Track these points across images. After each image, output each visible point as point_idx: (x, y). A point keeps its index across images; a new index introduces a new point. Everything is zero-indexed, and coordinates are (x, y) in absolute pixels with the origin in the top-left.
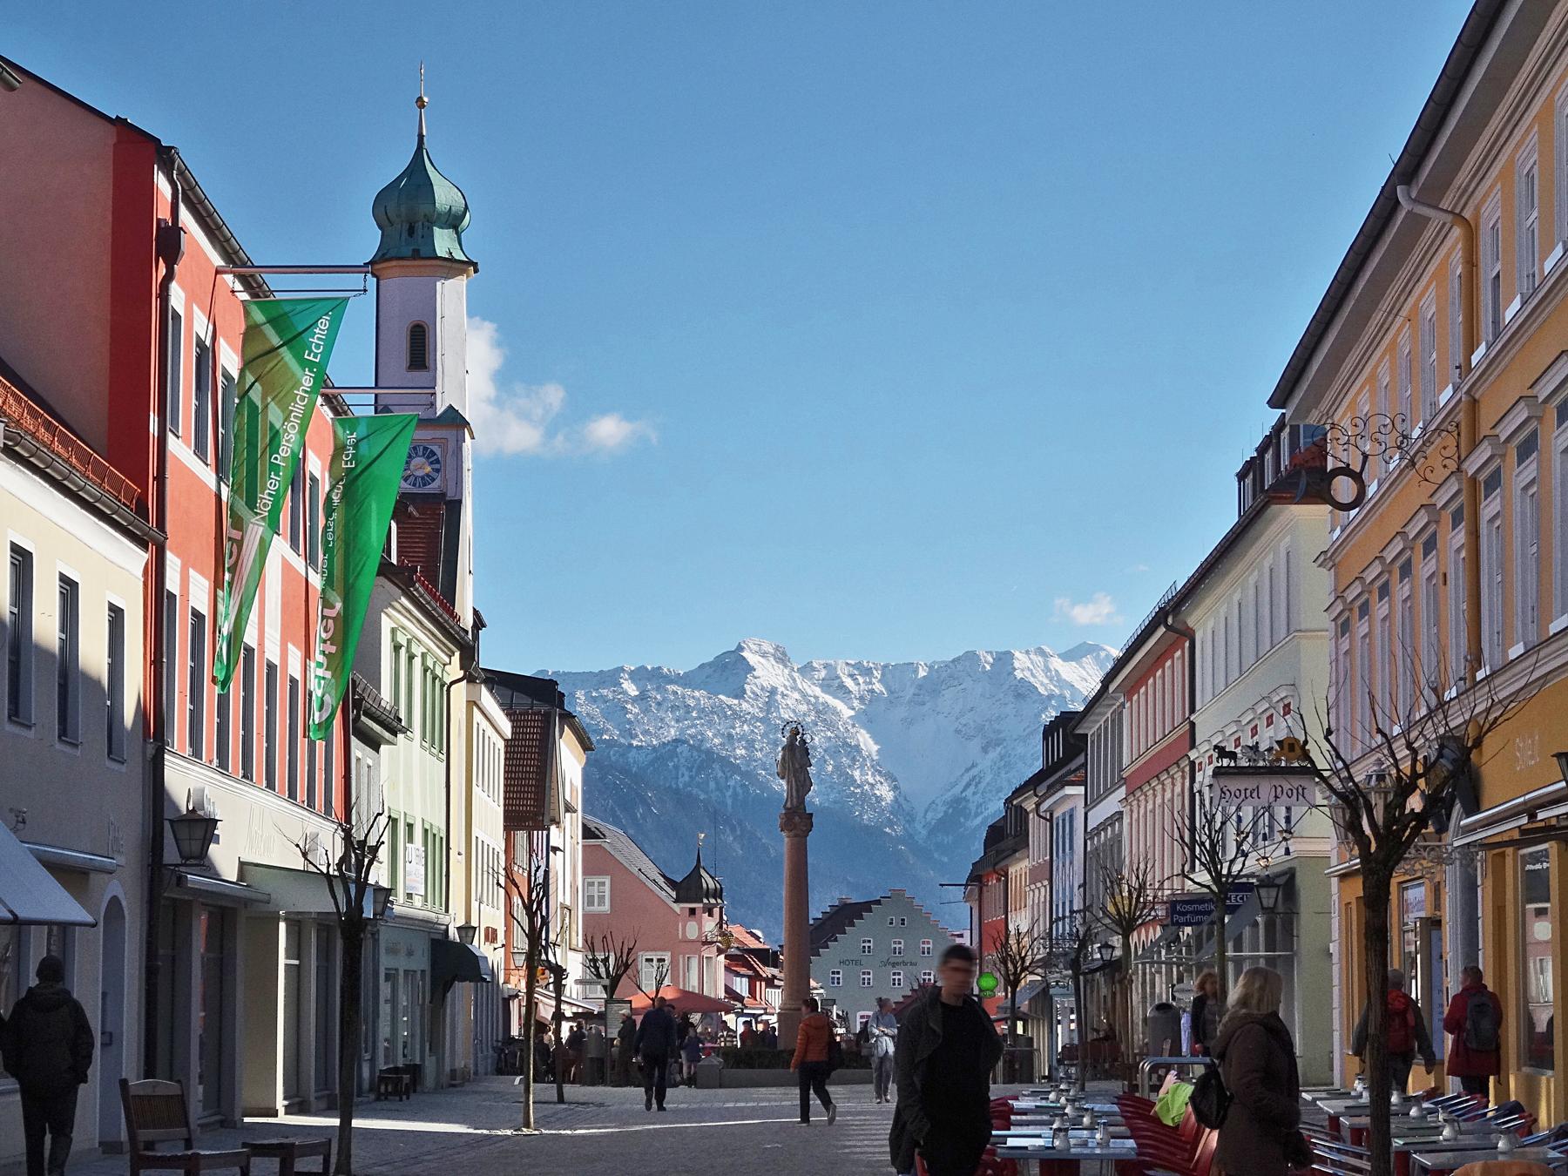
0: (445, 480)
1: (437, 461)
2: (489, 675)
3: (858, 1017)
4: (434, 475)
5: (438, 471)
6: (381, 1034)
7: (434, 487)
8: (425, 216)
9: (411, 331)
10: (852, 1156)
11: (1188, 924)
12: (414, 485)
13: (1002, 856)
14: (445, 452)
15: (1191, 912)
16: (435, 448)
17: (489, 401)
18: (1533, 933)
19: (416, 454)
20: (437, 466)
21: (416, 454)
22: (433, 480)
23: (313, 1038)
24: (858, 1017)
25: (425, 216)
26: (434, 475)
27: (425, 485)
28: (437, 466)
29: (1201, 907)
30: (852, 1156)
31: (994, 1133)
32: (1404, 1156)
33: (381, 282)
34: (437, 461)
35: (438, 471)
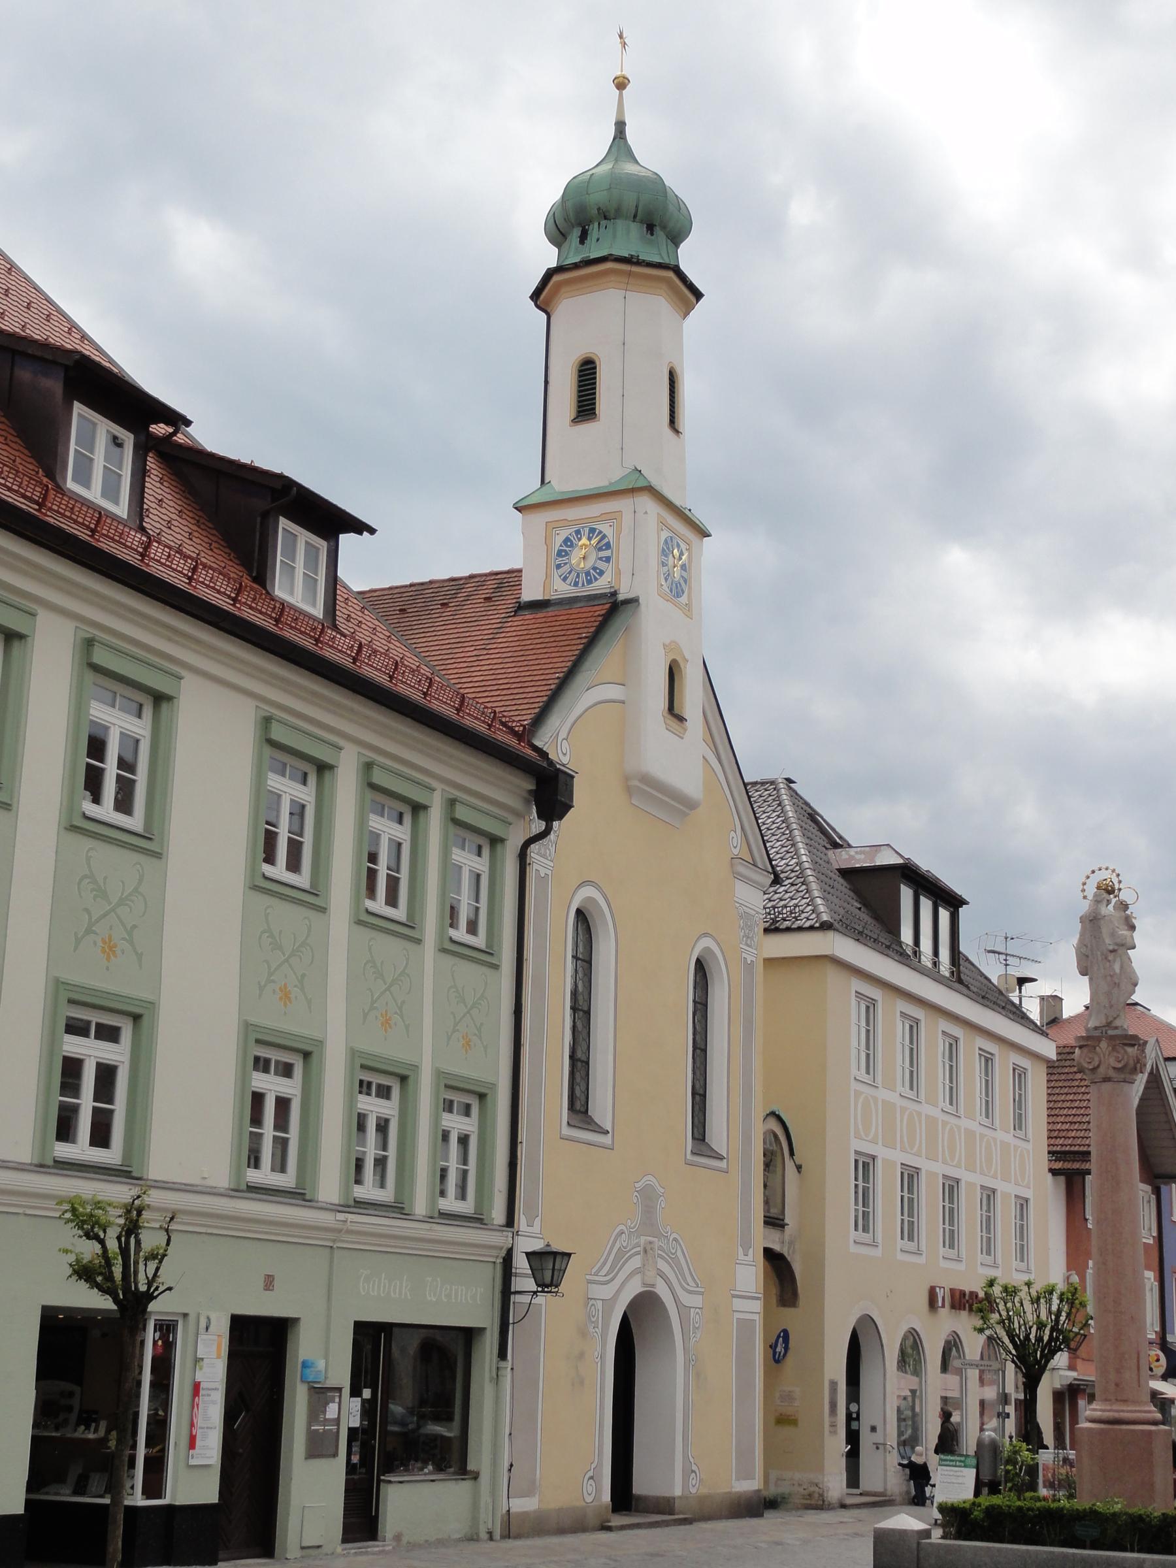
0: (618, 573)
5: (608, 559)
7: (601, 585)
19: (601, 559)
20: (607, 553)
21: (601, 559)
22: (601, 573)
26: (602, 565)
27: (590, 582)
28: (607, 553)
35: (608, 559)
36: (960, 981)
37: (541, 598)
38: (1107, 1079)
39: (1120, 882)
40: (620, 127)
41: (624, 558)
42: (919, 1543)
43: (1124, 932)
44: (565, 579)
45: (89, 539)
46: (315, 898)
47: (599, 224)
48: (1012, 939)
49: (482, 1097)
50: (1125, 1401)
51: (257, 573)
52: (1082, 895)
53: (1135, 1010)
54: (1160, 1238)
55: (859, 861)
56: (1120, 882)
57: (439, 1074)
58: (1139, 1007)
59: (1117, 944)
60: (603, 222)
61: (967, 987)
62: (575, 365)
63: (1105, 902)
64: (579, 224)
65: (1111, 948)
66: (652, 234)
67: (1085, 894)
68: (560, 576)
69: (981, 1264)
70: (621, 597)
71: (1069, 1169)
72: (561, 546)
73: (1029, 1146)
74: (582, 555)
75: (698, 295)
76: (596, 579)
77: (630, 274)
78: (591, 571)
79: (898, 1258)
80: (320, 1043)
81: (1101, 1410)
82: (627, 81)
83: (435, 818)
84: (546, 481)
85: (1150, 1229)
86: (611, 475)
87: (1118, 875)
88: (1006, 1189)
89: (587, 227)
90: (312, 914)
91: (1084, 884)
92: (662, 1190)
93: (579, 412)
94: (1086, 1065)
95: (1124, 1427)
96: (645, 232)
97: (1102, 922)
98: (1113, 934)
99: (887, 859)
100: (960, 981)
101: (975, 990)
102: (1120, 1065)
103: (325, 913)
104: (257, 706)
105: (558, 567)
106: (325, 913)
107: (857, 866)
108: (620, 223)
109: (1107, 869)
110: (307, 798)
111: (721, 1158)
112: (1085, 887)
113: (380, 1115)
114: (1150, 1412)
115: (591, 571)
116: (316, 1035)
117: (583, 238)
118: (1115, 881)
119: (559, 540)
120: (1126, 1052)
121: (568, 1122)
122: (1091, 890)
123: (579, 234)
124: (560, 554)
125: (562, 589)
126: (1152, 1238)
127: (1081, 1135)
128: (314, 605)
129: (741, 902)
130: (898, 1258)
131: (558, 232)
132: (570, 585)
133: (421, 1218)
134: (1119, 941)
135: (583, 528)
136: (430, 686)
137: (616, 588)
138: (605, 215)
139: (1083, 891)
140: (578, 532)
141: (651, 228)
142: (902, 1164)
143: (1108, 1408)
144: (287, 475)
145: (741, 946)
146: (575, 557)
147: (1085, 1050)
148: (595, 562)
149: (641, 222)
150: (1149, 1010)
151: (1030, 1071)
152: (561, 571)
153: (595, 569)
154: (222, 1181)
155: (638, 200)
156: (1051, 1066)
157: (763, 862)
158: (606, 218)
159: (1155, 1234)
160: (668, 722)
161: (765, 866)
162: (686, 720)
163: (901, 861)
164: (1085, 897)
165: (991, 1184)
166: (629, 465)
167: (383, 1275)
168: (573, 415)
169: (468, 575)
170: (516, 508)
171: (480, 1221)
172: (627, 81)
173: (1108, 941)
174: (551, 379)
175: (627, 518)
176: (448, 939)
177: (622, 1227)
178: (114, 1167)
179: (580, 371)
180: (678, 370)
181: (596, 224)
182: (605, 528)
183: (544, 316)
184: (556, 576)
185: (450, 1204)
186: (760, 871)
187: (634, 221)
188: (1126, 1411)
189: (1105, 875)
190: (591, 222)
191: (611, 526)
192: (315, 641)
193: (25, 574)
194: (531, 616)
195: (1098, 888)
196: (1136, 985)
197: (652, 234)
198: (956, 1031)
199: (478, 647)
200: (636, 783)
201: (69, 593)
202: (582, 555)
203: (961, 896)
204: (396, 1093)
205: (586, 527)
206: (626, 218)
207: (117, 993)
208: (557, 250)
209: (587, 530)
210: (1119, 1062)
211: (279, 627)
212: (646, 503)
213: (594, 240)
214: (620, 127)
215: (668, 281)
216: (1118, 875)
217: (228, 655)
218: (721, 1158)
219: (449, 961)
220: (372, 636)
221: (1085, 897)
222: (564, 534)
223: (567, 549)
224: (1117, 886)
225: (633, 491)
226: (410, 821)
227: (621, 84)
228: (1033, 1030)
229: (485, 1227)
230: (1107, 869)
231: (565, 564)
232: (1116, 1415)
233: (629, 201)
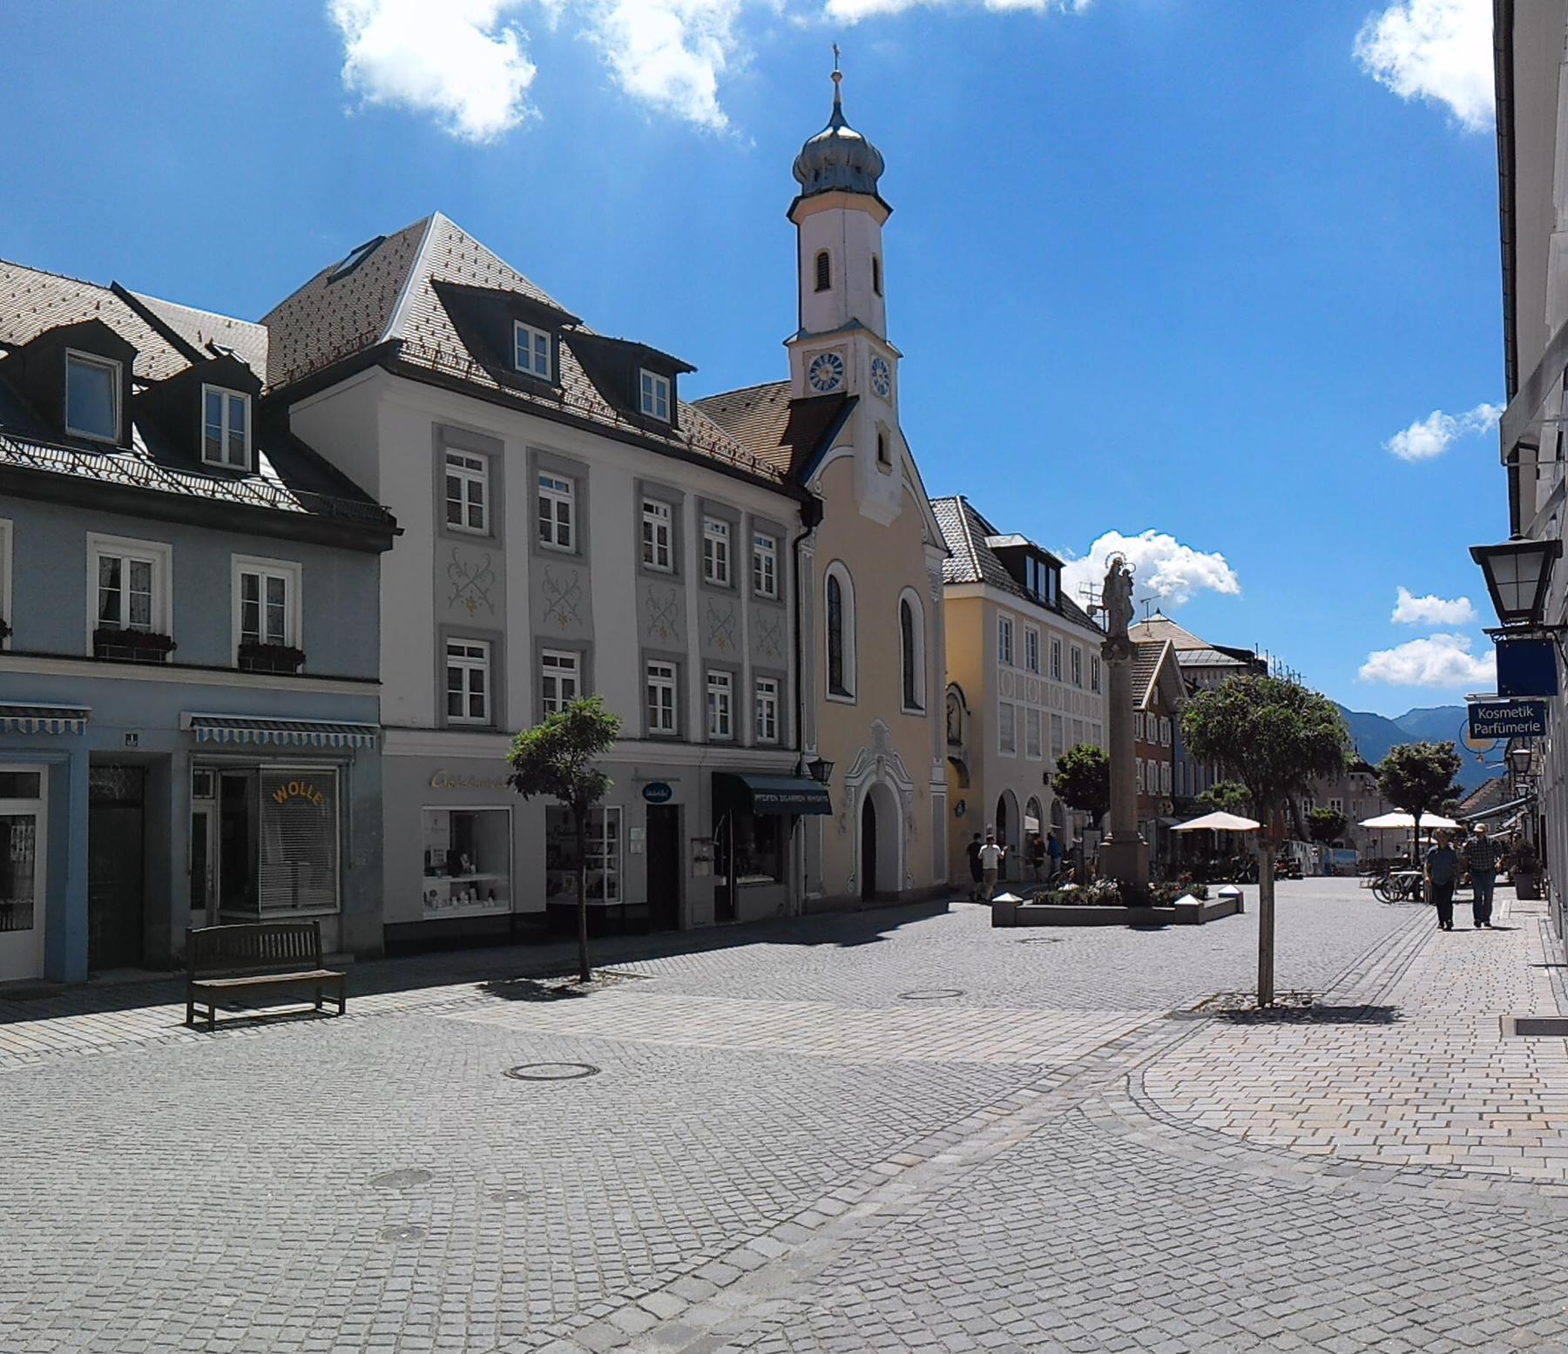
1: (840, 365)
2: (1223, 777)
4: (837, 376)
5: (840, 373)
6: (686, 834)
7: (837, 389)
8: (825, 159)
9: (819, 259)
12: (822, 389)
13: (894, 400)
15: (1499, 720)
16: (837, 354)
17: (522, 89)
22: (837, 381)
25: (825, 159)
26: (837, 376)
27: (830, 387)
29: (1512, 714)
31: (1216, 848)
33: (802, 227)
34: (840, 365)
35: (840, 373)
40: (837, 106)
41: (850, 374)
105: (812, 378)
152: (814, 381)
163: (1026, 543)
180: (878, 259)
214: (837, 106)
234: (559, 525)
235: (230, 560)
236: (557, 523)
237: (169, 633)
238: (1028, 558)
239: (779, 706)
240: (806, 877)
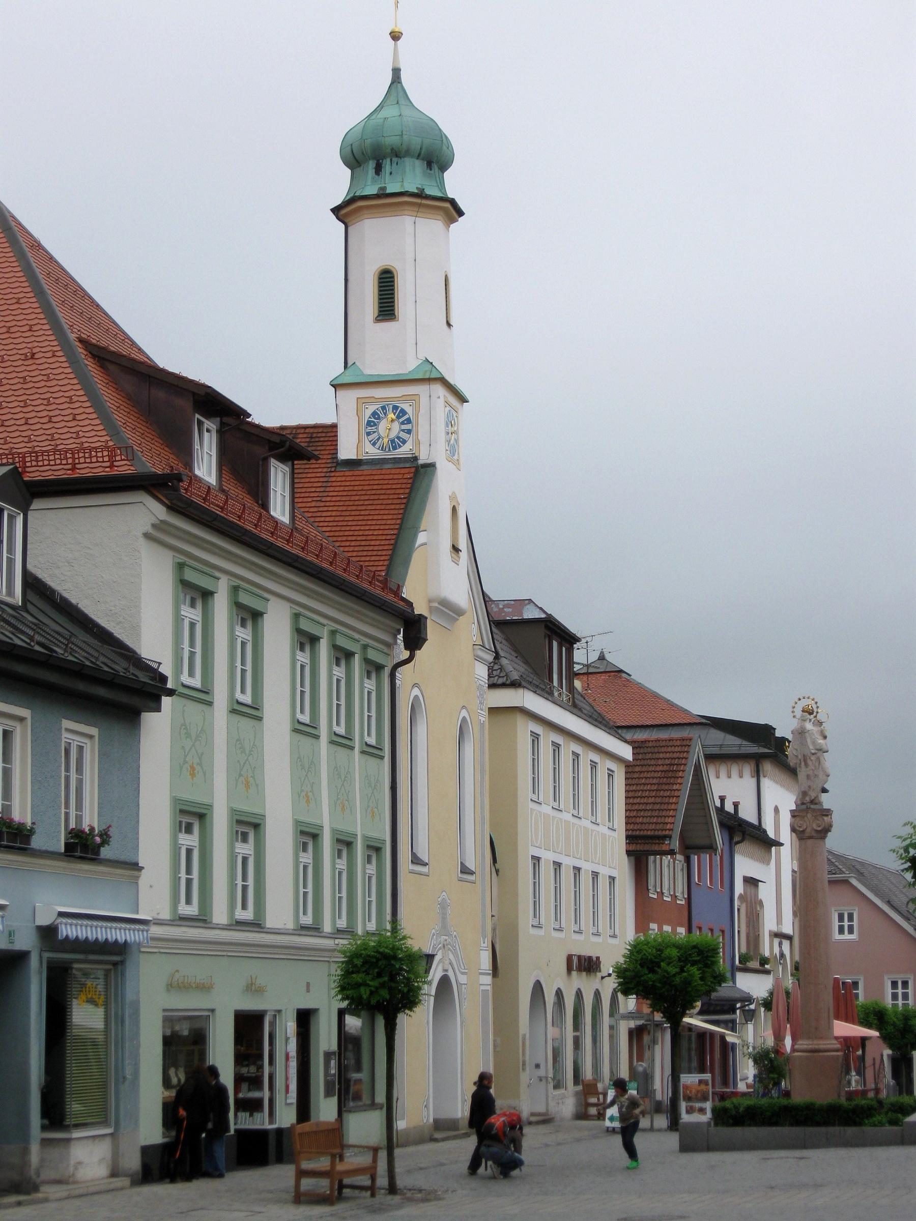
0: (418, 443)
1: (409, 421)
3: (842, 937)
5: (409, 432)
7: (404, 451)
10: (137, 411)
11: (744, 1094)
14: (417, 411)
18: (71, 1019)
19: (403, 430)
20: (408, 427)
21: (403, 430)
22: (404, 442)
23: (183, 547)
24: (842, 937)
26: (404, 435)
27: (395, 448)
28: (408, 427)
30: (137, 411)
32: (748, 1086)
34: (409, 421)
35: (409, 432)
36: (575, 705)
37: (355, 458)
38: (811, 837)
39: (818, 707)
40: (396, 72)
41: (422, 431)
42: (708, 1130)
43: (821, 741)
44: (374, 444)
45: (238, 522)
46: (350, 741)
47: (391, 160)
48: (578, 649)
49: (201, 817)
50: (821, 1038)
51: (262, 501)
52: (792, 715)
53: (620, 677)
54: (689, 900)
55: (508, 614)
56: (818, 707)
57: (334, 831)
58: (624, 675)
59: (818, 750)
60: (395, 160)
61: (580, 710)
62: (377, 273)
63: (808, 721)
64: (374, 158)
65: (813, 751)
66: (431, 170)
67: (795, 714)
68: (370, 442)
69: (532, 926)
70: (421, 462)
71: (641, 851)
72: (370, 417)
73: (615, 834)
74: (388, 428)
75: (460, 213)
76: (400, 447)
77: (420, 205)
78: (396, 439)
79: (531, 933)
80: (210, 807)
81: (807, 1045)
82: (401, 35)
83: (324, 647)
84: (350, 363)
85: (683, 893)
86: (410, 366)
87: (816, 703)
88: (605, 872)
89: (381, 161)
90: (204, 707)
91: (794, 707)
92: (449, 901)
93: (380, 311)
94: (798, 828)
95: (821, 1054)
96: (426, 168)
97: (807, 734)
98: (814, 743)
99: (530, 613)
100: (575, 705)
101: (586, 712)
102: (819, 829)
103: (211, 705)
104: (174, 556)
105: (368, 434)
106: (211, 705)
107: (508, 618)
108: (408, 162)
109: (808, 698)
110: (340, 675)
111: (425, 864)
112: (794, 709)
113: (189, 847)
114: (834, 1044)
115: (396, 439)
116: (205, 800)
117: (378, 169)
118: (814, 706)
119: (368, 413)
120: (824, 820)
121: (412, 861)
122: (798, 713)
123: (374, 166)
124: (369, 424)
125: (372, 452)
126: (684, 900)
127: (648, 821)
128: (284, 515)
129: (478, 677)
130: (531, 933)
131: (352, 157)
132: (379, 449)
133: (291, 932)
134: (818, 747)
135: (388, 405)
136: (348, 564)
137: (417, 455)
138: (397, 154)
139: (793, 712)
140: (383, 408)
141: (429, 164)
142: (592, 872)
143: (811, 1043)
144: (185, 375)
145: (479, 711)
146: (383, 426)
147: (798, 819)
148: (399, 433)
149: (423, 159)
150: (630, 675)
151: (599, 764)
152: (370, 438)
153: (398, 438)
154: (290, 925)
155: (422, 142)
156: (628, 765)
157: (490, 647)
158: (397, 156)
159: (686, 896)
160: (453, 555)
161: (490, 647)
162: (461, 551)
163: (543, 616)
164: (794, 717)
165: (578, 864)
166: (422, 357)
167: (699, 1004)
168: (376, 314)
169: (279, 425)
170: (332, 385)
171: (259, 925)
172: (401, 35)
173: (811, 747)
174: (350, 277)
175: (424, 401)
176: (235, 701)
177: (433, 931)
178: (192, 917)
179: (380, 278)
180: (449, 276)
181: (388, 160)
182: (405, 406)
183: (343, 226)
184: (367, 443)
185: (240, 915)
186: (486, 650)
187: (417, 159)
188: (822, 1044)
189: (809, 702)
190: (384, 157)
191: (411, 405)
192: (238, 517)
193: (214, 553)
194: (351, 473)
195: (803, 711)
196: (828, 776)
197: (431, 170)
198: (538, 729)
199: (315, 499)
200: (436, 605)
201: (235, 563)
202: (388, 428)
203: (575, 635)
204: (196, 829)
205: (390, 404)
206: (412, 156)
207: (193, 801)
208: (349, 171)
209: (391, 407)
210: (819, 826)
211: (290, 546)
212: (439, 391)
213: (388, 172)
214: (396, 72)
215: (445, 210)
216: (816, 703)
217: (329, 599)
218: (425, 864)
219: (237, 718)
220: (142, 440)
221: (794, 717)
222: (372, 409)
223: (375, 421)
224: (815, 710)
225: (429, 380)
226: (201, 608)
227: (395, 36)
228: (619, 739)
229: (262, 930)
230: (808, 698)
231: (374, 432)
232: (816, 1047)
233: (416, 143)
234: (76, 777)
235: (202, 685)
236: (75, 776)
237: (29, 822)
238: (285, 519)
239: (365, 919)
240: (397, 1099)
